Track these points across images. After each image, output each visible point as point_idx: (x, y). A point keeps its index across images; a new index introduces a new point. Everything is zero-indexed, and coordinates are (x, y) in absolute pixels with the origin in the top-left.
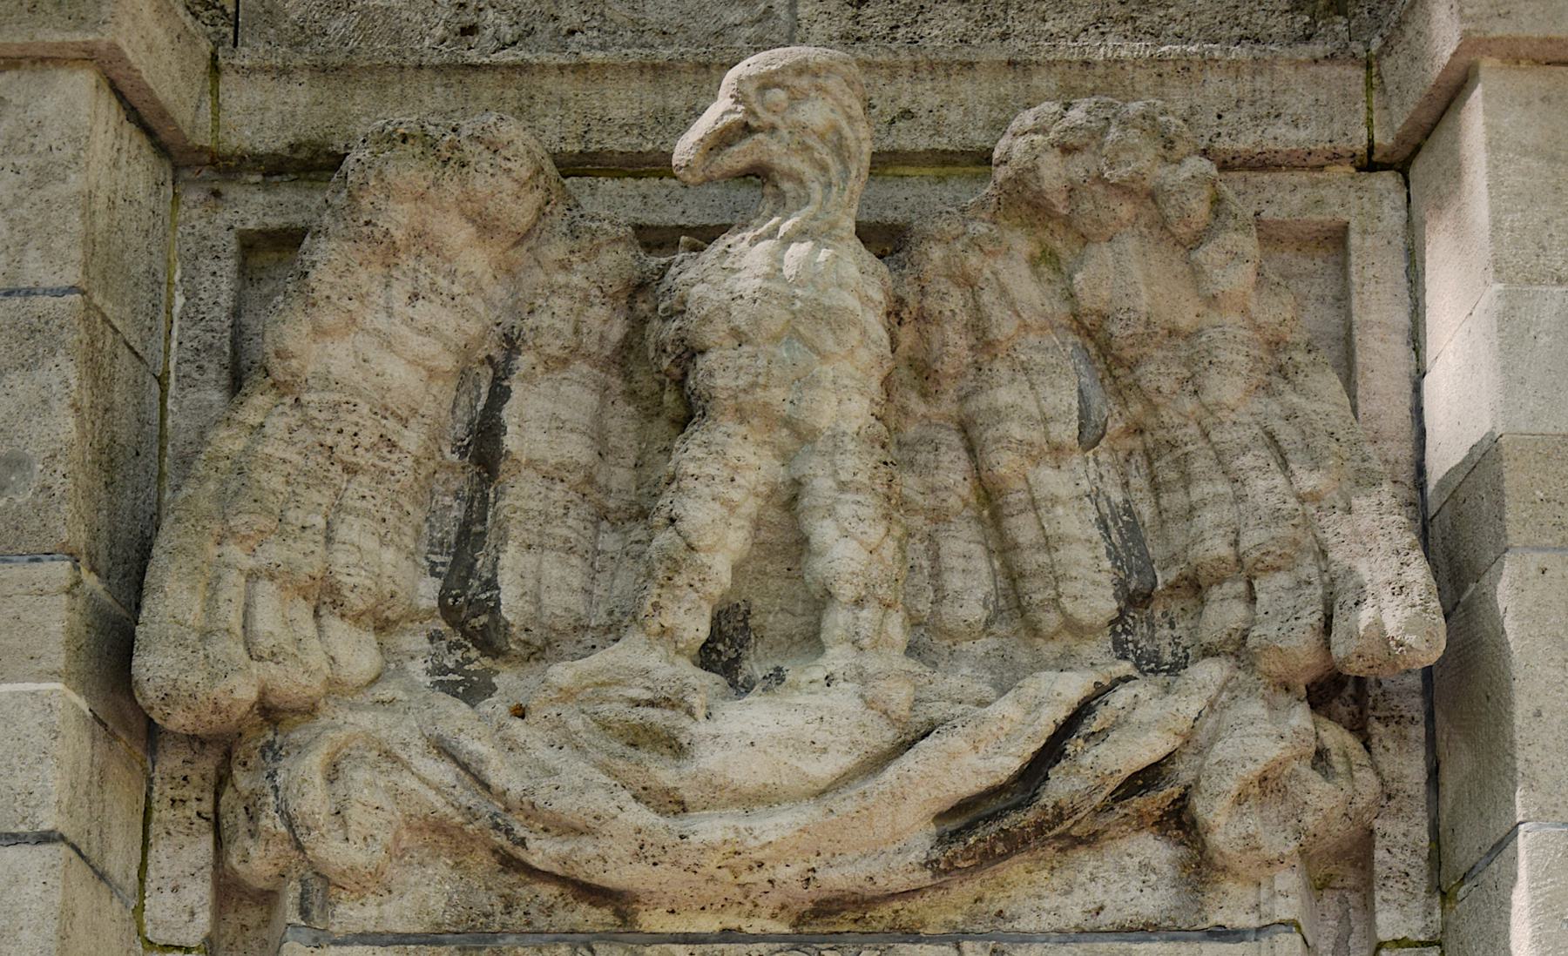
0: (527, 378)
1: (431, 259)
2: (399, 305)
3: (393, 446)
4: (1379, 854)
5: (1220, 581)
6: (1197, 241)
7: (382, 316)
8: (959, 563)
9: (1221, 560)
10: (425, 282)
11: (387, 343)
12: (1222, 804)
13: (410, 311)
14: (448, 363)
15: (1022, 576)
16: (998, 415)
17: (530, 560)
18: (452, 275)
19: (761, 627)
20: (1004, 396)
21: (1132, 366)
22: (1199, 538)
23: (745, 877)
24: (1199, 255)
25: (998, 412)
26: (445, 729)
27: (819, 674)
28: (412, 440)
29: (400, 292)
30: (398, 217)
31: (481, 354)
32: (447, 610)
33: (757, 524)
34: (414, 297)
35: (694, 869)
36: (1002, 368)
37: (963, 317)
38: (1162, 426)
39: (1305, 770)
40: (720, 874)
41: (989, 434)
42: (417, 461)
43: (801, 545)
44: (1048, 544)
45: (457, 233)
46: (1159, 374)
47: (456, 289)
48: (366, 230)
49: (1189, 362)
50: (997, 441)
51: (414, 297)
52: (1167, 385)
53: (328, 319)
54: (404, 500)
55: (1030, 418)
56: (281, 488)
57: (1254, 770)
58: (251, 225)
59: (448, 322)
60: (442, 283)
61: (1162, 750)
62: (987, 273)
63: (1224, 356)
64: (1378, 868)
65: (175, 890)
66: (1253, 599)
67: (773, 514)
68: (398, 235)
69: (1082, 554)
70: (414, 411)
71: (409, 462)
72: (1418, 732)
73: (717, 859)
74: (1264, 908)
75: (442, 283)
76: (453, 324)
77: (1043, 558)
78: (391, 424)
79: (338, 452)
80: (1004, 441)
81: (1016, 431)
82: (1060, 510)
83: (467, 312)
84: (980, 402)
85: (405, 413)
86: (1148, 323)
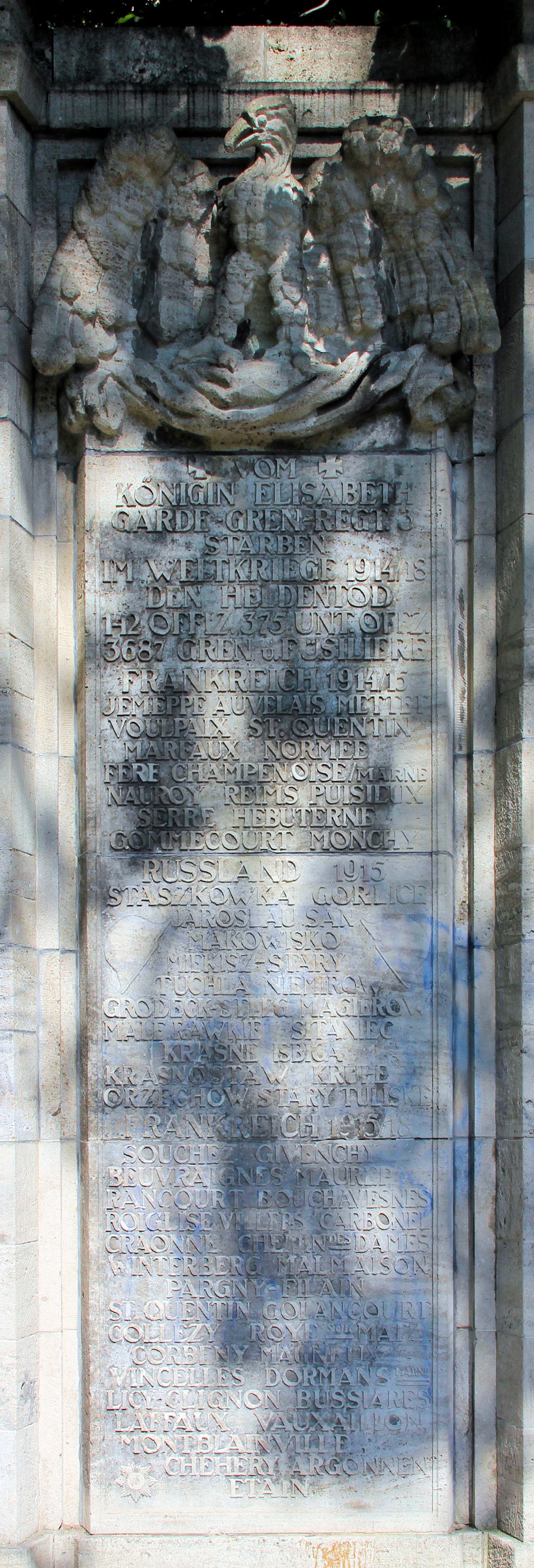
0: (169, 229)
1: (134, 182)
2: (122, 202)
3: (120, 257)
4: (475, 420)
5: (421, 313)
6: (417, 178)
7: (117, 206)
8: (325, 303)
9: (422, 305)
10: (132, 192)
11: (119, 217)
12: (419, 404)
13: (127, 204)
14: (140, 223)
15: (349, 309)
16: (342, 245)
17: (171, 303)
18: (142, 188)
19: (254, 329)
20: (344, 237)
21: (392, 225)
22: (414, 296)
23: (249, 432)
24: (417, 184)
25: (342, 244)
26: (142, 374)
27: (276, 352)
28: (127, 254)
29: (123, 195)
30: (122, 168)
31: (152, 218)
32: (140, 323)
33: (254, 290)
34: (128, 197)
35: (231, 429)
36: (343, 226)
37: (329, 205)
38: (401, 249)
39: (450, 390)
40: (241, 431)
41: (338, 252)
42: (129, 263)
43: (270, 302)
44: (358, 297)
45: (144, 171)
46: (403, 230)
47: (143, 194)
48: (111, 172)
49: (413, 225)
50: (341, 255)
51: (128, 197)
52: (404, 234)
53: (97, 208)
54: (124, 279)
55: (353, 246)
56: (81, 276)
57: (431, 391)
58: (62, 158)
59: (139, 206)
60: (138, 191)
61: (399, 382)
62: (339, 187)
63: (425, 224)
64: (474, 425)
65: (44, 433)
66: (433, 322)
67: (259, 287)
68: (123, 174)
69: (371, 301)
70: (128, 244)
71: (126, 264)
72: (490, 371)
73: (239, 426)
74: (433, 442)
75: (138, 191)
76: (142, 207)
77: (357, 302)
78: (119, 249)
79: (101, 262)
80: (344, 256)
81: (349, 252)
82: (364, 283)
83: (147, 203)
84: (335, 239)
85: (124, 244)
86: (398, 210)
